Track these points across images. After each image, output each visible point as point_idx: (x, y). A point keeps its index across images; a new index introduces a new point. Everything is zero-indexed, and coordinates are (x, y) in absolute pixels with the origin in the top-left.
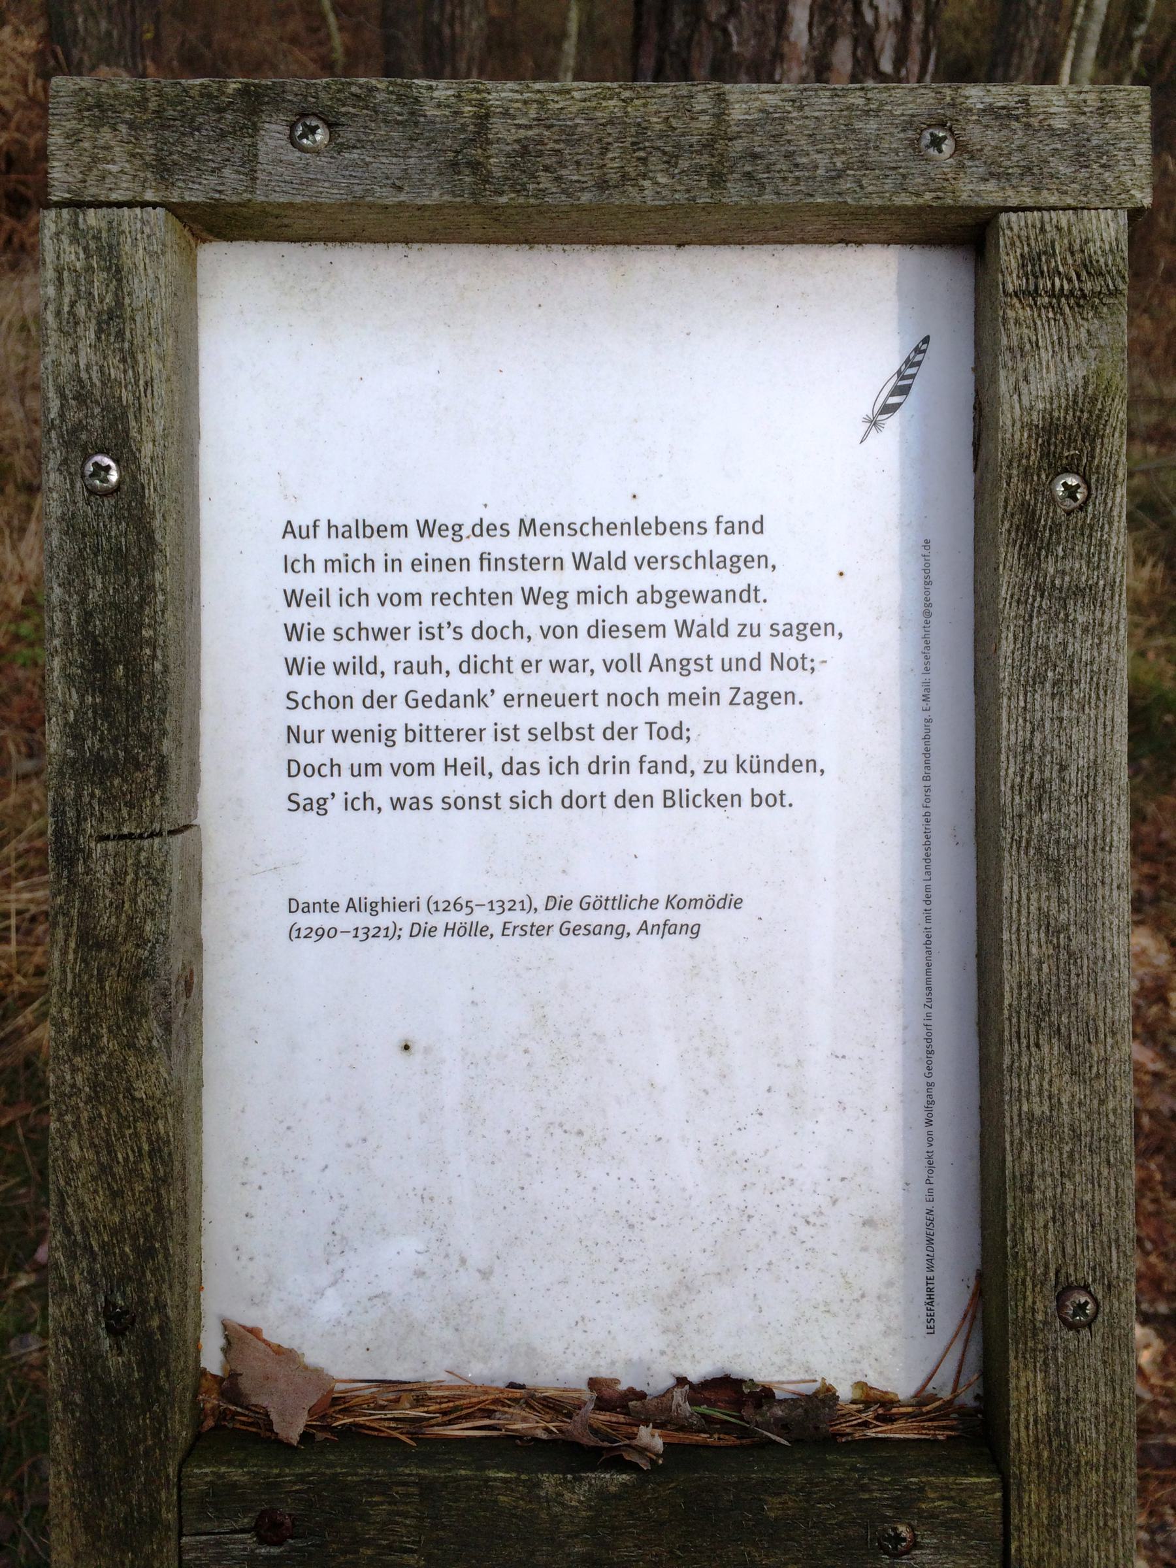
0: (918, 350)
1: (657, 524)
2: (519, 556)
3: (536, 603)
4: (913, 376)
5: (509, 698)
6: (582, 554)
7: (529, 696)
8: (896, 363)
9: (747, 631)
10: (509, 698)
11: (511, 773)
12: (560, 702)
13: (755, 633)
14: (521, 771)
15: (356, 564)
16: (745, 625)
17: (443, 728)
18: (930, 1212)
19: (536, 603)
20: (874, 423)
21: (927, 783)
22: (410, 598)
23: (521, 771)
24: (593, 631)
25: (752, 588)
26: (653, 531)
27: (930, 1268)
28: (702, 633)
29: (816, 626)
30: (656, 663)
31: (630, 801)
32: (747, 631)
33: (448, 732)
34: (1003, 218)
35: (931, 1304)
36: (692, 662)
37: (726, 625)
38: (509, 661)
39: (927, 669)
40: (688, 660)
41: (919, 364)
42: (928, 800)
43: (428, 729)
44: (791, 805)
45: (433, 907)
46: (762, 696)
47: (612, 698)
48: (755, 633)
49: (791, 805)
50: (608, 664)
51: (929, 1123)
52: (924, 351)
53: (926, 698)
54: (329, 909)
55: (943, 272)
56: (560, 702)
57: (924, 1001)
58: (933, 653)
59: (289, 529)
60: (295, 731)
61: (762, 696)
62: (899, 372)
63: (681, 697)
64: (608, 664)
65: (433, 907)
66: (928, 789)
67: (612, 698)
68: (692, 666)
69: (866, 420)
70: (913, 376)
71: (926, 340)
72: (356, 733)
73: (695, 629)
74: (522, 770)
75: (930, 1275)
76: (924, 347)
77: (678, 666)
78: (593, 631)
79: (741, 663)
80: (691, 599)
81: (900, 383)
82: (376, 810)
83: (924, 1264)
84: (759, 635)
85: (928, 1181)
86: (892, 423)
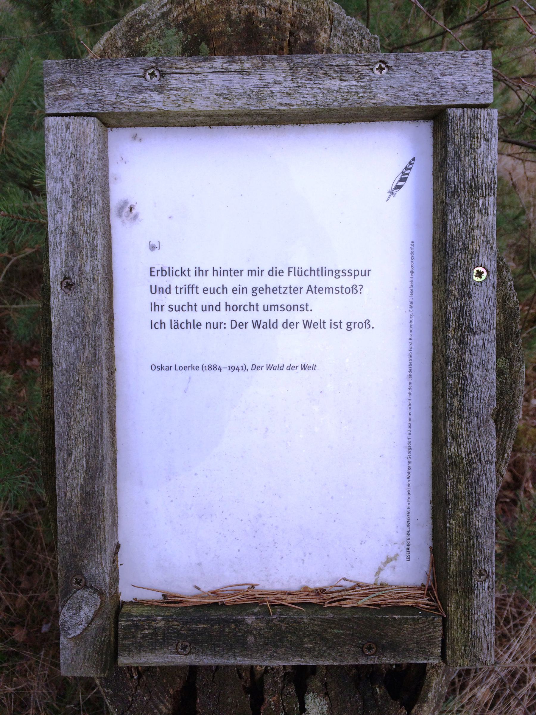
0: (410, 163)
2: (338, 321)
3: (310, 327)
4: (408, 174)
5: (235, 289)
6: (307, 321)
8: (402, 168)
10: (235, 289)
12: (212, 292)
17: (233, 269)
18: (408, 513)
19: (310, 327)
22: (327, 289)
25: (359, 280)
27: (408, 535)
28: (176, 327)
29: (261, 289)
30: (310, 289)
31: (290, 325)
33: (321, 289)
34: (449, 110)
35: (408, 549)
36: (341, 272)
37: (220, 306)
39: (412, 295)
40: (339, 271)
41: (410, 169)
42: (411, 347)
45: (204, 369)
47: (208, 325)
51: (409, 477)
52: (413, 164)
53: (411, 306)
54: (232, 274)
55: (424, 130)
56: (212, 292)
58: (414, 288)
59: (310, 289)
62: (402, 172)
63: (254, 272)
65: (204, 369)
66: (411, 343)
67: (208, 325)
68: (341, 274)
70: (408, 174)
71: (414, 159)
72: (236, 272)
73: (262, 325)
76: (413, 162)
77: (334, 274)
79: (211, 307)
81: (403, 177)
85: (408, 501)
86: (399, 193)
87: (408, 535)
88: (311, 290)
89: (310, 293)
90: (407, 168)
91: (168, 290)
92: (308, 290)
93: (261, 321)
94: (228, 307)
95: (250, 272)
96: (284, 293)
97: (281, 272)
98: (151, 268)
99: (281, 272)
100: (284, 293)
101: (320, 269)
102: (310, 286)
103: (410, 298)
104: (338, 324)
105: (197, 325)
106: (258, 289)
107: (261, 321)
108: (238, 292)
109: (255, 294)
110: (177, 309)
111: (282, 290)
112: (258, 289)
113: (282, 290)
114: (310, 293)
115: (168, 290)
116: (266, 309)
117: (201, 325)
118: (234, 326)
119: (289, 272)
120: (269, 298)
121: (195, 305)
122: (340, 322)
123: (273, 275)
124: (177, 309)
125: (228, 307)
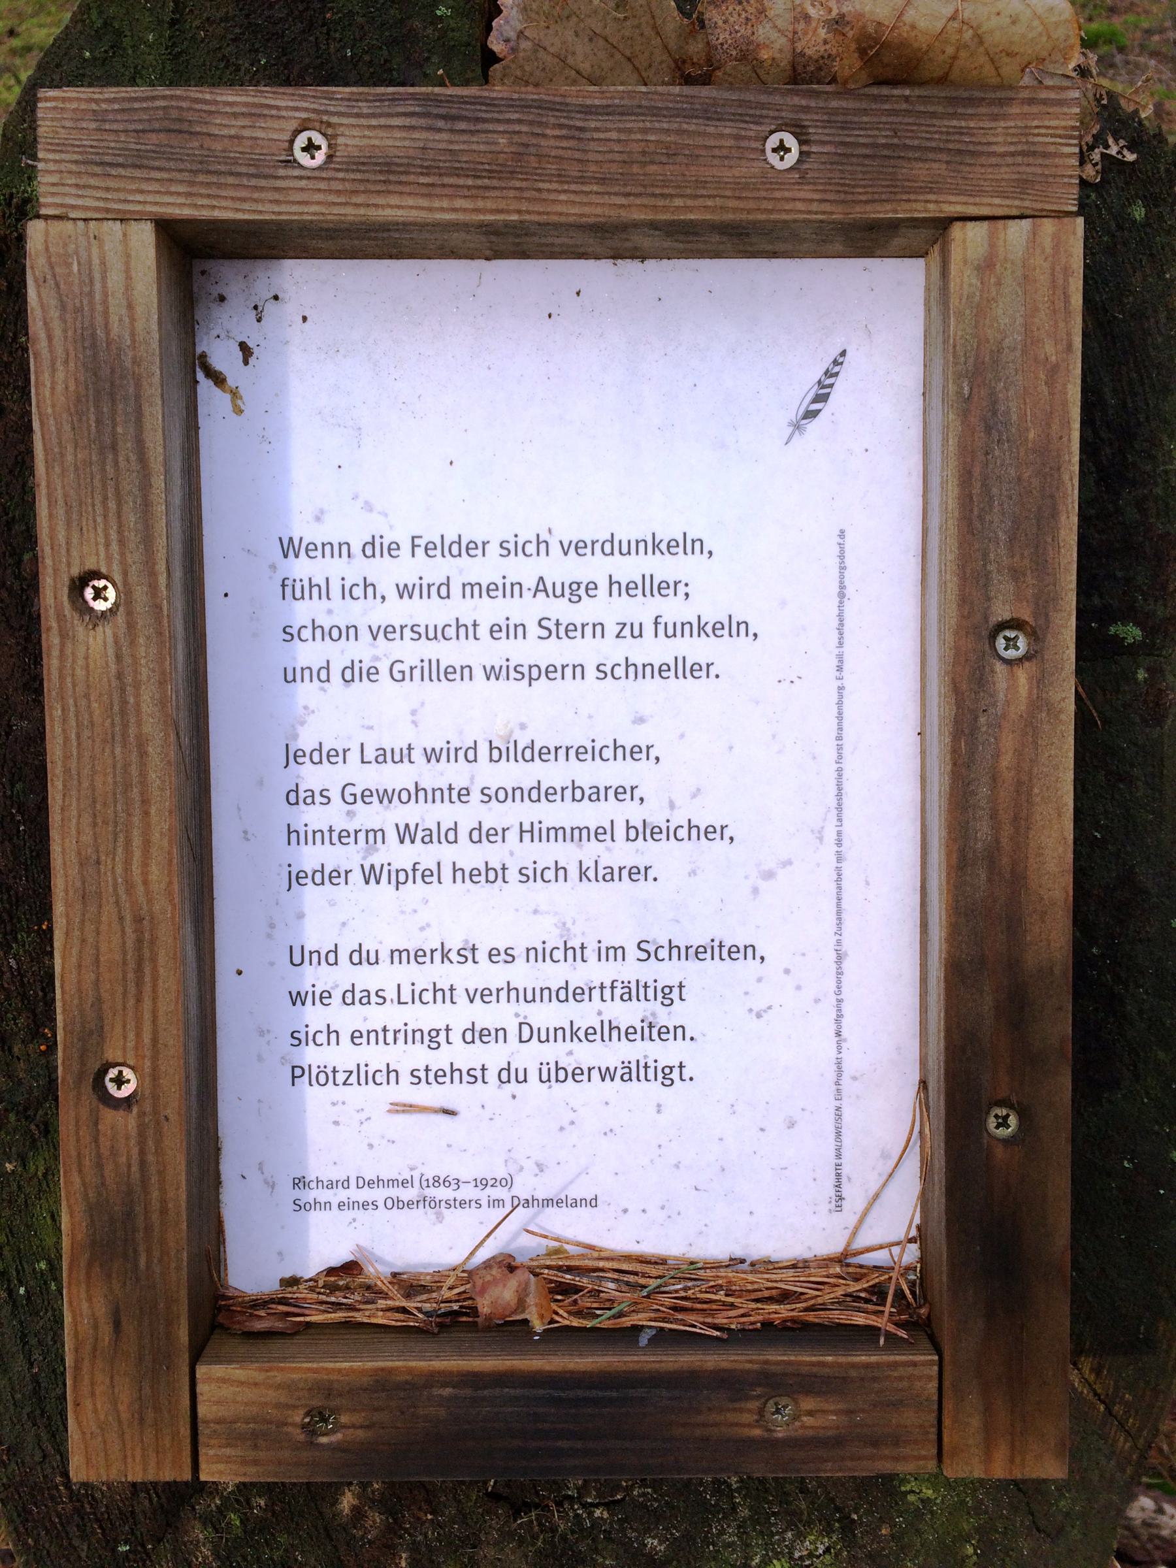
0: (836, 363)
1: (487, 870)
7: (594, 625)
8: (818, 373)
9: (627, 632)
11: (353, 1003)
13: (636, 633)
14: (365, 1000)
15: (679, 831)
16: (625, 624)
18: (838, 1109)
20: (797, 427)
21: (840, 743)
23: (365, 1000)
24: (504, 1075)
25: (642, 984)
26: (483, 878)
27: (839, 1156)
30: (541, 587)
32: (627, 632)
38: (452, 989)
41: (837, 374)
42: (840, 756)
43: (721, 946)
44: (691, 1079)
45: (424, 1184)
46: (575, 587)
47: (532, 953)
48: (636, 633)
49: (691, 1079)
50: (472, 993)
53: (840, 668)
54: (655, 1035)
57: (835, 930)
59: (541, 587)
60: (410, 589)
61: (575, 587)
62: (819, 382)
64: (472, 993)
65: (424, 1184)
67: (532, 953)
69: (790, 424)
70: (831, 386)
71: (843, 353)
73: (420, 834)
74: (366, 999)
75: (839, 1161)
77: (427, 1038)
78: (504, 1075)
80: (375, 799)
82: (706, 554)
83: (833, 1153)
84: (641, 635)
86: (813, 426)
87: (839, 1156)
88: (545, 590)
89: (541, 595)
90: (828, 374)
91: (332, 955)
92: (537, 590)
93: (301, 539)
94: (459, 874)
95: (468, 589)
96: (344, 1084)
97: (393, 549)
98: (413, 538)
99: (393, 549)
100: (344, 1084)
101: (651, 1064)
102: (541, 578)
103: (837, 651)
104: (478, 1074)
105: (692, 670)
106: (583, 587)
107: (301, 539)
108: (500, 593)
109: (576, 598)
110: (431, 635)
111: (341, 1077)
112: (583, 587)
113: (341, 1077)
114: (541, 595)
115: (332, 955)
116: (520, 629)
117: (398, 548)
118: (361, 1185)
119: (414, 546)
120: (646, 604)
121: (475, 625)
122: (483, 1069)
123: (374, 556)
124: (431, 635)
125: (459, 874)
